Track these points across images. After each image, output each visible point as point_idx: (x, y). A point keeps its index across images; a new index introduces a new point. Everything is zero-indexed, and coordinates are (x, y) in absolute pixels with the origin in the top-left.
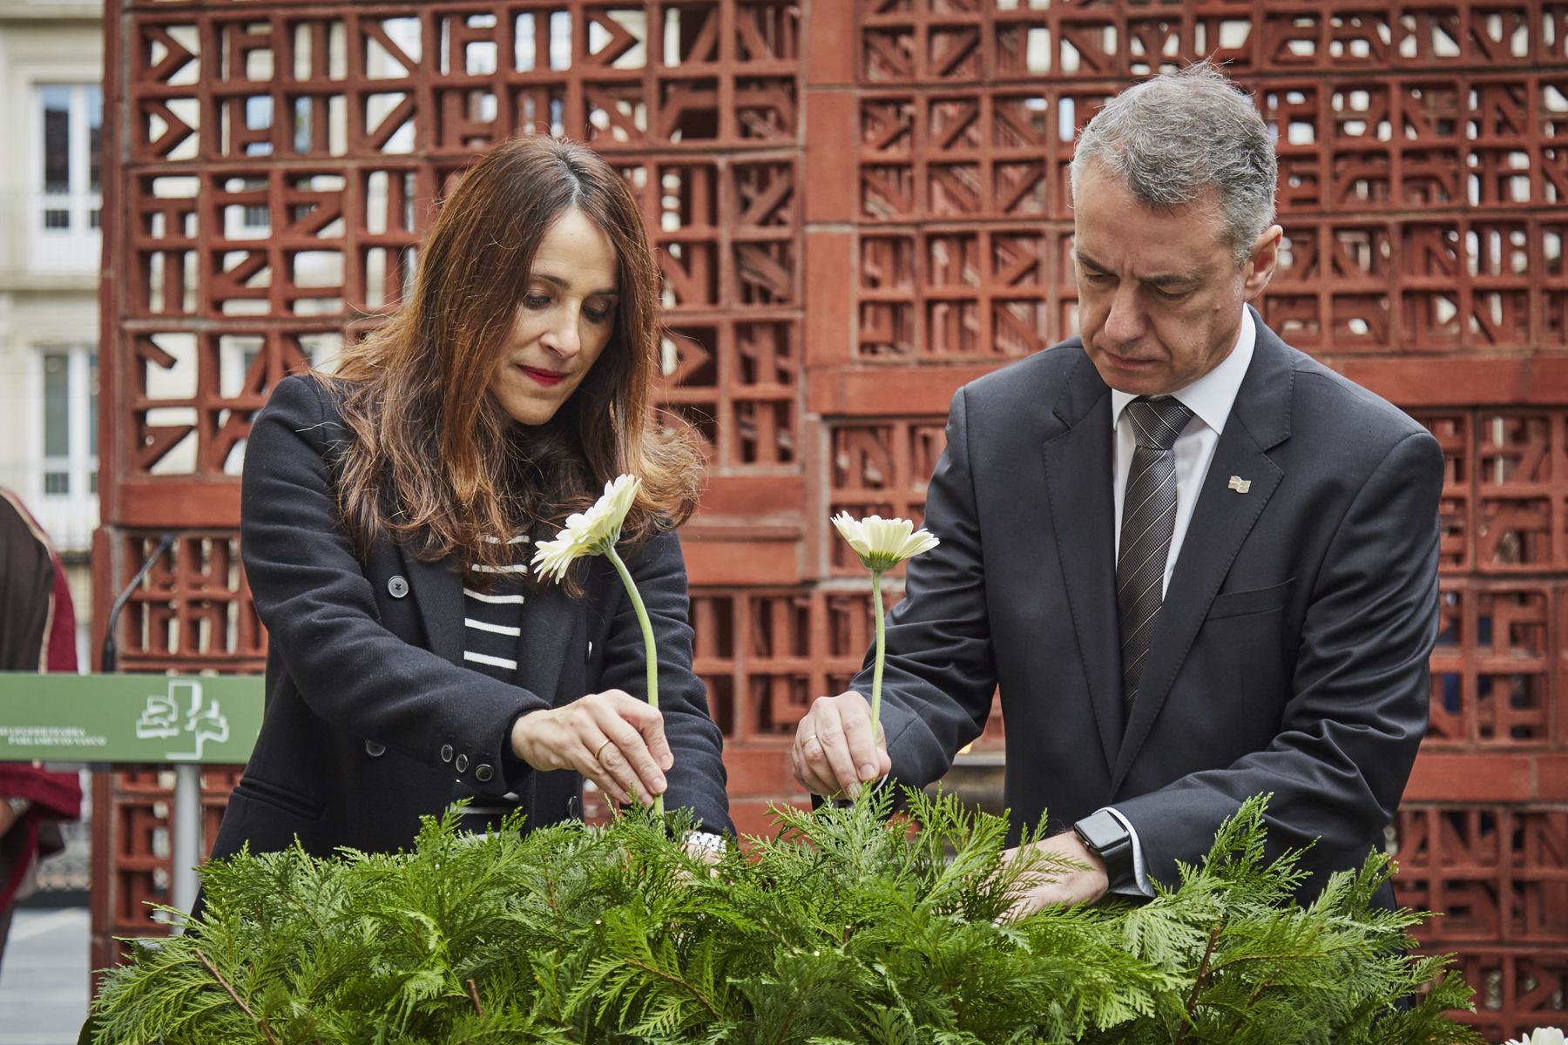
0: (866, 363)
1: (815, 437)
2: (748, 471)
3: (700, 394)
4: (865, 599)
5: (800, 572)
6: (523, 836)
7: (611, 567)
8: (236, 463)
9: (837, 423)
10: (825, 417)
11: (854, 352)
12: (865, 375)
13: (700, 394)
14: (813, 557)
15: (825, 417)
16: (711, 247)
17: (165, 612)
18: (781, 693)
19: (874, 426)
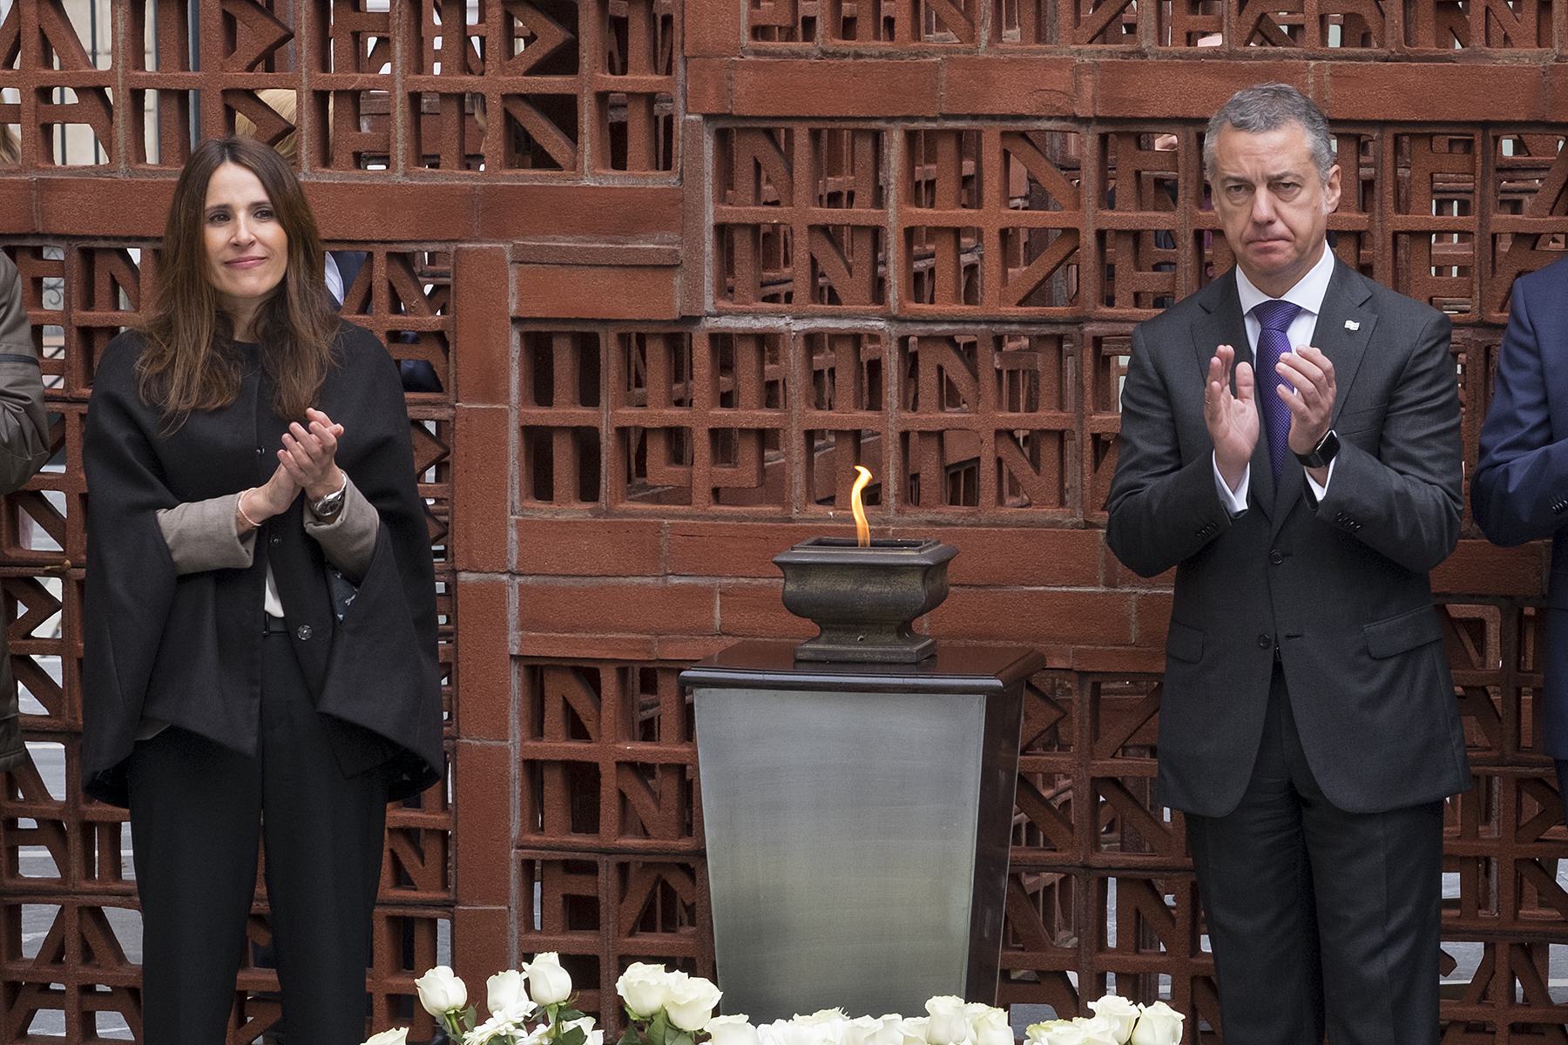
0: (757, 53)
1: (698, 143)
2: (615, 180)
3: (555, 84)
4: (766, 342)
5: (679, 306)
6: (303, 492)
7: (493, 401)
8: (440, 587)
9: (721, 124)
10: (708, 117)
11: (745, 39)
12: (756, 67)
13: (555, 84)
14: (694, 290)
15: (708, 117)
16: (586, 441)
17: (35, 267)
18: (657, 452)
19: (771, 131)
